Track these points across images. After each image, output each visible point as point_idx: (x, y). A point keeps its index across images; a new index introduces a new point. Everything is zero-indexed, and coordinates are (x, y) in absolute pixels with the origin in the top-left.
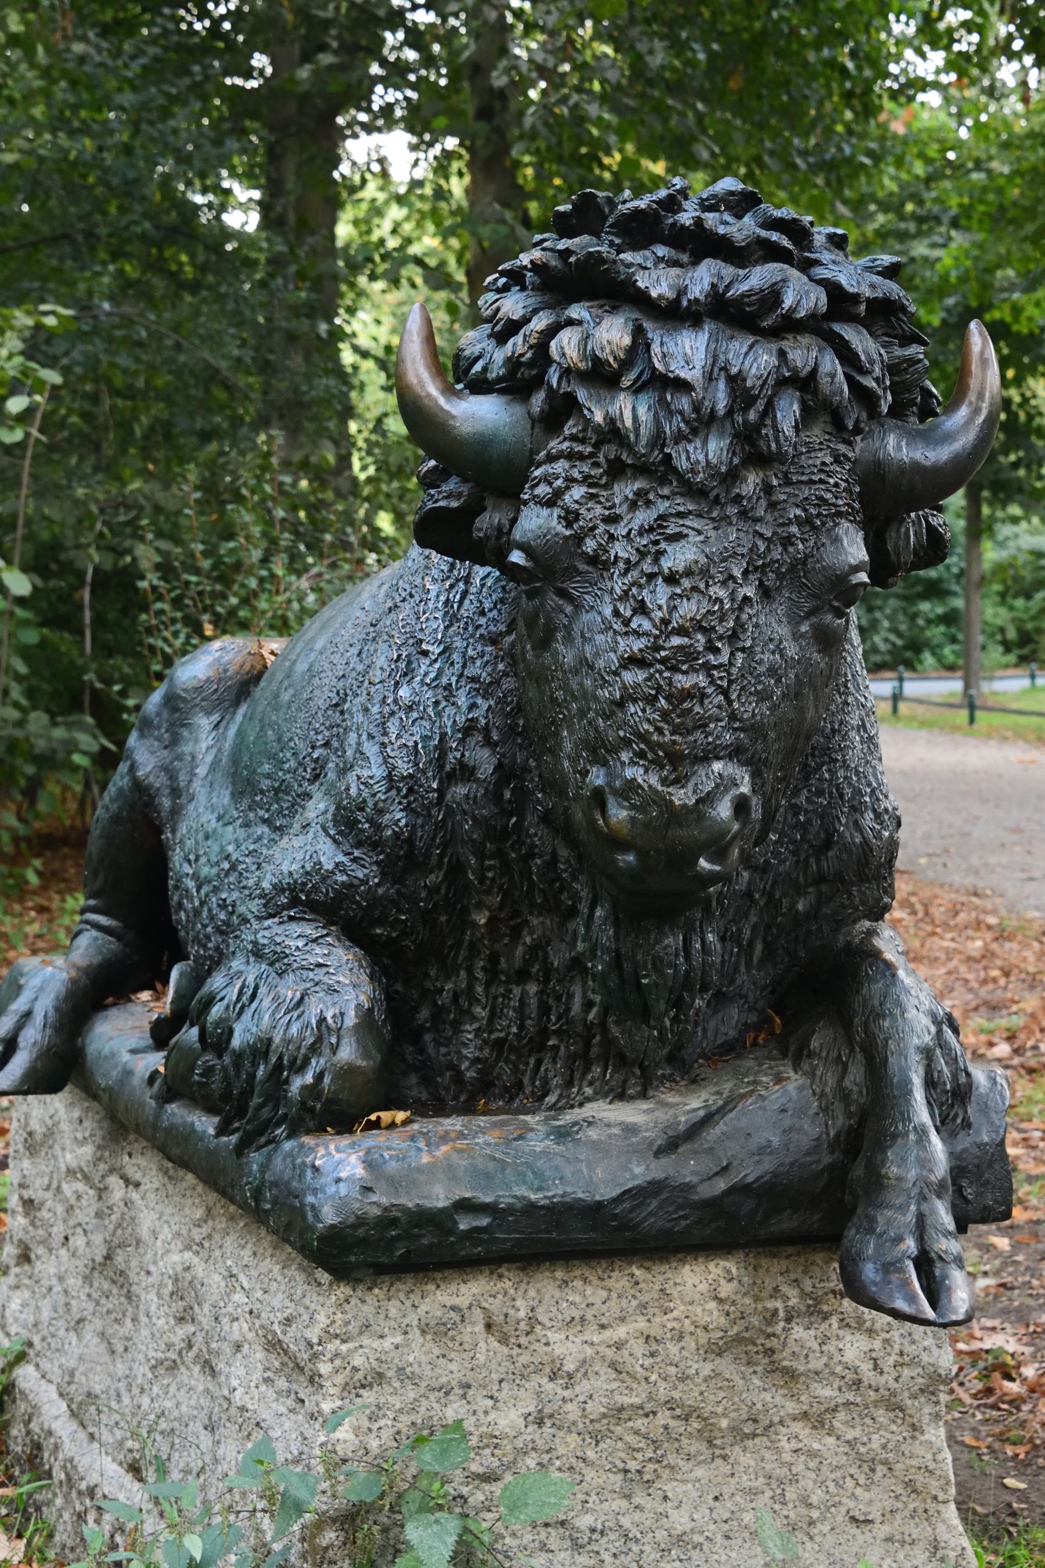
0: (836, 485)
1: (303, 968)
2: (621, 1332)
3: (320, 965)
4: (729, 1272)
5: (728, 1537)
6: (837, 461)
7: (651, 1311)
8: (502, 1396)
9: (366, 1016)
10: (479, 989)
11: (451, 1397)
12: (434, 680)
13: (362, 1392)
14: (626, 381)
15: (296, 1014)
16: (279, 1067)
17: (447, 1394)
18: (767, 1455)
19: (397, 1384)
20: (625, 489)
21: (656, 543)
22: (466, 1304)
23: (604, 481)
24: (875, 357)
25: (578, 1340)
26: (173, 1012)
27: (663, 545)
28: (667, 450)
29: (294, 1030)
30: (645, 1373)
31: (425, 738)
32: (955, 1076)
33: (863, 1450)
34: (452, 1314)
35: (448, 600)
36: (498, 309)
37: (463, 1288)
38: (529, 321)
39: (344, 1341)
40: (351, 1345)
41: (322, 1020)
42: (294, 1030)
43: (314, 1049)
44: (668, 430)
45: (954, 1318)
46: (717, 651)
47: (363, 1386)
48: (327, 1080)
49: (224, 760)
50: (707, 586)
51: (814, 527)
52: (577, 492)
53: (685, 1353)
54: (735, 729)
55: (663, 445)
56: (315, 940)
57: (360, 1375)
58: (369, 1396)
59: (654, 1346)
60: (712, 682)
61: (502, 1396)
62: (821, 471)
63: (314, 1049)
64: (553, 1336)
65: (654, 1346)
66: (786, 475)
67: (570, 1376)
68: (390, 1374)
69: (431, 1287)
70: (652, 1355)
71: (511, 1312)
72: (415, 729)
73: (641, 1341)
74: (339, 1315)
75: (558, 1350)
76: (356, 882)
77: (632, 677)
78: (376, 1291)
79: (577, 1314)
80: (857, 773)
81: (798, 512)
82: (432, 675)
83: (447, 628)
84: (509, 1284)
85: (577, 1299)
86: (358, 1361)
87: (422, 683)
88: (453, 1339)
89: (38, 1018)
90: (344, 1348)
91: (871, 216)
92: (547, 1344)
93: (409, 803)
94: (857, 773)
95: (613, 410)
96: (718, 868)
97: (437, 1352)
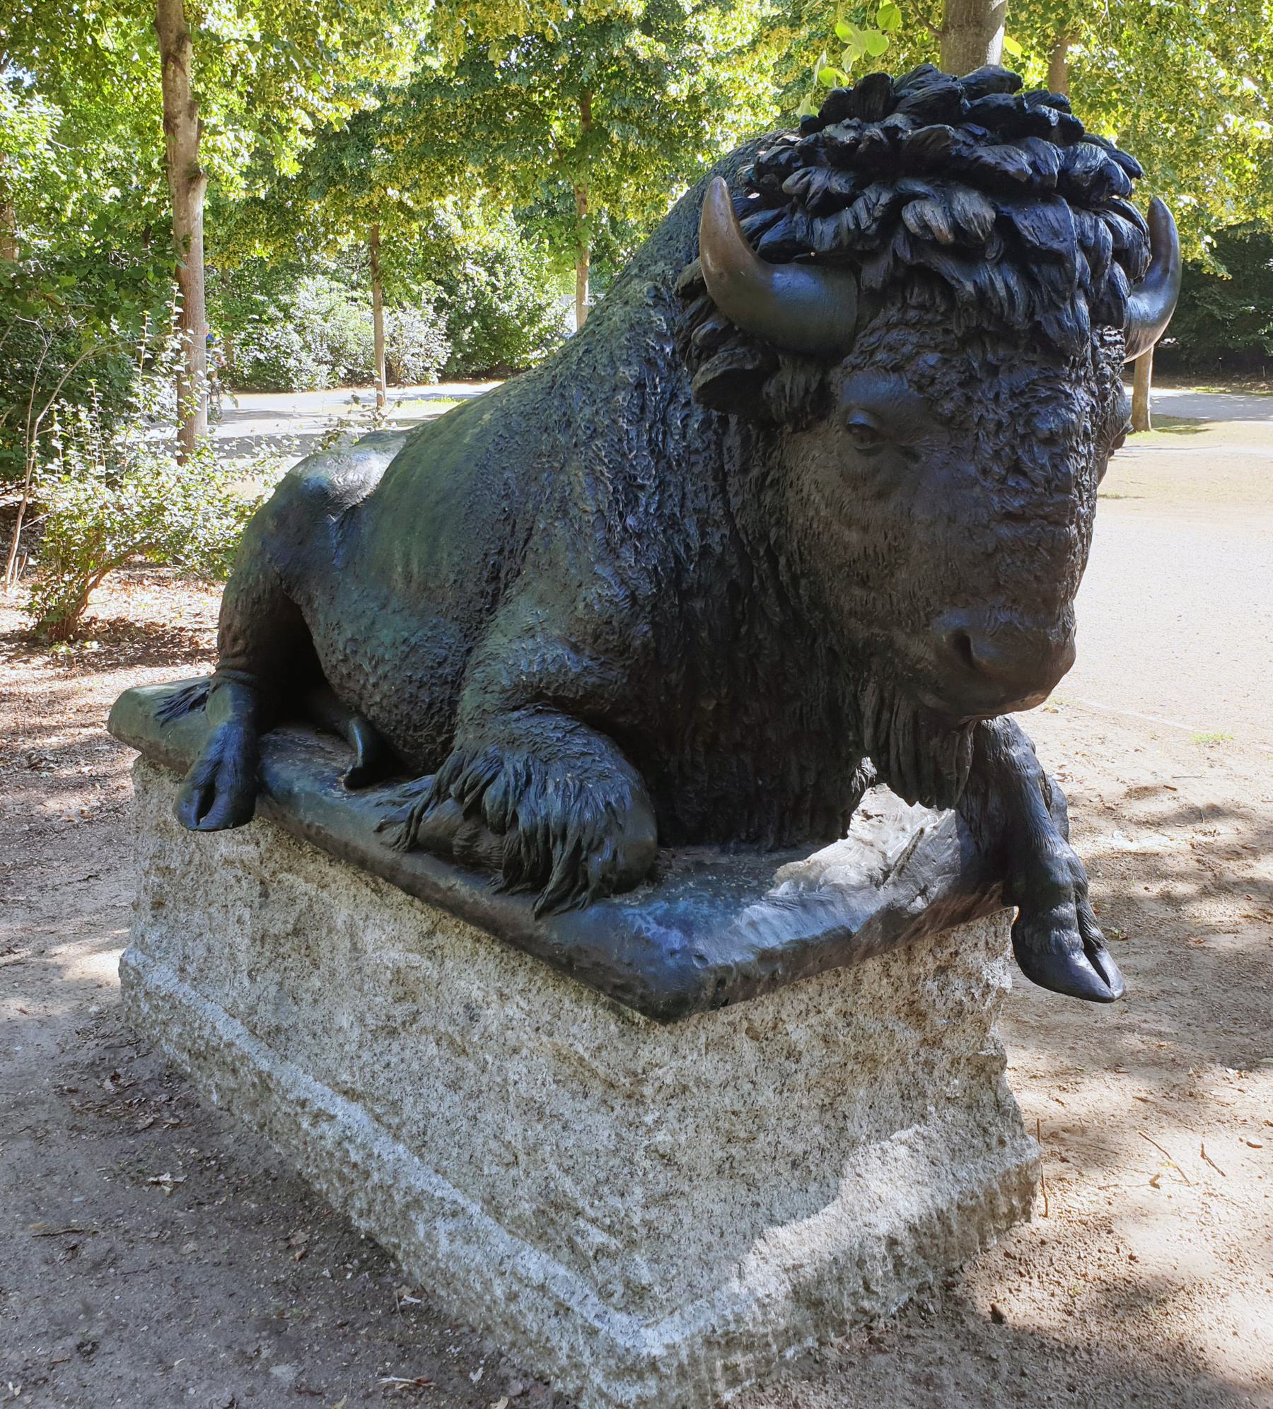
1: (569, 756)
3: (584, 754)
10: (701, 759)
12: (656, 510)
13: (671, 1101)
16: (578, 849)
18: (901, 1070)
19: (695, 1090)
21: (1027, 405)
26: (365, 763)
27: (1035, 408)
28: (1037, 318)
35: (650, 441)
36: (809, 184)
40: (665, 1069)
43: (607, 831)
48: (620, 858)
56: (571, 731)
64: (790, 1028)
68: (691, 1084)
70: (849, 1025)
72: (651, 554)
73: (841, 1016)
75: (794, 1037)
76: (606, 683)
77: (1005, 531)
83: (657, 463)
87: (646, 512)
88: (728, 1046)
90: (660, 1072)
95: (983, 278)
97: (717, 1058)
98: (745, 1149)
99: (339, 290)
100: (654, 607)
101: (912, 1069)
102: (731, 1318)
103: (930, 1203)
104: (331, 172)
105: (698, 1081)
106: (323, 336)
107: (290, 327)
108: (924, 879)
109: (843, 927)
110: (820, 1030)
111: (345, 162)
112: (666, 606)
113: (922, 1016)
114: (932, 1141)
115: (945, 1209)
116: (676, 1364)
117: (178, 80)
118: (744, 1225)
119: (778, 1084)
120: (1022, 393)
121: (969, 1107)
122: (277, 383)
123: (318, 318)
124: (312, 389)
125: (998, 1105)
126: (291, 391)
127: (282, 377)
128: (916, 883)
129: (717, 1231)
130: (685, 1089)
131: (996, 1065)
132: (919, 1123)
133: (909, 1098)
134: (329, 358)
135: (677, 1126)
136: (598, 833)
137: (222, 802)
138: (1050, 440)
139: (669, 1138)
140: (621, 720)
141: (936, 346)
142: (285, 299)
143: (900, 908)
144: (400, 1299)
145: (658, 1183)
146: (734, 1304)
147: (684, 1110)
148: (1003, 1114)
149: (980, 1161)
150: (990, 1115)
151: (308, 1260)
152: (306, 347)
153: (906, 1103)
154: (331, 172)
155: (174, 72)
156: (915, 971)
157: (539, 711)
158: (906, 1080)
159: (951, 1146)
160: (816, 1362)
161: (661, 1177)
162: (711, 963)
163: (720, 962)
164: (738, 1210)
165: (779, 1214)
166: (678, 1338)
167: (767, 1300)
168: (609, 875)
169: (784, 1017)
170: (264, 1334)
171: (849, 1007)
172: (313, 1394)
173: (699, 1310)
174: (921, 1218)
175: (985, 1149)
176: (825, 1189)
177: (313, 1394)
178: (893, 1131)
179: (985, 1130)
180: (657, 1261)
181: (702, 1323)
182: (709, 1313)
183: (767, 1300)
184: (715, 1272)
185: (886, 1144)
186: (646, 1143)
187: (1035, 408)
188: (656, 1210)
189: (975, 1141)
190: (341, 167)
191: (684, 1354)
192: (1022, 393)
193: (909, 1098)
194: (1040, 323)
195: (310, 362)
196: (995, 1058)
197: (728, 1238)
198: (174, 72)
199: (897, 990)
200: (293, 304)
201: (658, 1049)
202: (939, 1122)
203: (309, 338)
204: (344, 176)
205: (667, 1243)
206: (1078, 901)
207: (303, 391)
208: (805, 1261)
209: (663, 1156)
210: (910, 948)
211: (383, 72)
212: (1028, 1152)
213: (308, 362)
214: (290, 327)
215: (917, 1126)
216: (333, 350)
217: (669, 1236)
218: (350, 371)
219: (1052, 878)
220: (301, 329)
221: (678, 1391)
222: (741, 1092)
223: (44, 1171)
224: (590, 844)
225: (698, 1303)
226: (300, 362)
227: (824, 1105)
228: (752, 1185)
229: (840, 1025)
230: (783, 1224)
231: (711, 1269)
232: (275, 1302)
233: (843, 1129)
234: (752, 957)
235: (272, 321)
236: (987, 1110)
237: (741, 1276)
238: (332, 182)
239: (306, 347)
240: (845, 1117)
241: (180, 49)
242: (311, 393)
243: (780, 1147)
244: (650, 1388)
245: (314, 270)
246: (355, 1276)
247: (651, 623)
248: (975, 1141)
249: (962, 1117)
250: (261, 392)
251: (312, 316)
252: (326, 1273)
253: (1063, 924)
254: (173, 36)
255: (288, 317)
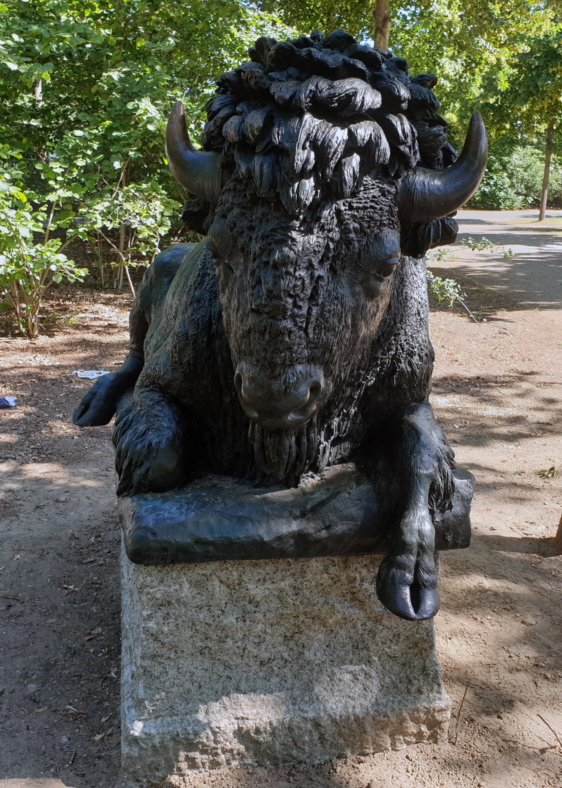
0: (381, 209)
2: (283, 584)
3: (156, 416)
4: (333, 561)
5: (331, 661)
6: (384, 195)
7: (296, 576)
8: (226, 610)
9: (172, 443)
11: (203, 610)
12: (210, 288)
14: (259, 149)
15: (140, 440)
17: (200, 609)
18: (352, 630)
19: (177, 605)
20: (259, 211)
21: (270, 244)
22: (209, 573)
23: (248, 206)
24: (410, 134)
25: (262, 588)
27: (273, 246)
28: (277, 190)
29: (139, 447)
30: (293, 602)
31: (203, 316)
32: (446, 485)
33: (395, 630)
34: (203, 577)
37: (208, 567)
38: (218, 112)
39: (151, 588)
40: (155, 589)
41: (150, 444)
42: (139, 447)
44: (278, 178)
45: (425, 616)
46: (300, 307)
47: (161, 605)
48: (150, 473)
49: (153, 306)
50: (295, 271)
51: (365, 233)
52: (236, 211)
53: (312, 594)
54: (311, 348)
55: (276, 188)
57: (160, 601)
58: (164, 610)
59: (298, 591)
60: (296, 325)
61: (226, 610)
62: (372, 201)
63: (147, 457)
64: (250, 586)
65: (298, 591)
66: (350, 204)
67: (258, 602)
68: (173, 601)
69: (192, 566)
70: (296, 594)
71: (231, 577)
74: (149, 578)
78: (166, 568)
79: (261, 577)
80: (412, 337)
81: (356, 225)
82: (210, 286)
84: (229, 565)
85: (262, 571)
86: (158, 596)
89: (98, 397)
90: (151, 590)
91: (308, 33)
92: (247, 590)
93: (194, 347)
94: (412, 337)
96: (300, 417)
97: (196, 592)
98: (218, 645)
99: (538, 155)
100: (195, 341)
101: (360, 632)
102: (191, 731)
103: (350, 710)
104: (531, 89)
105: (178, 601)
106: (523, 180)
107: (505, 174)
108: (329, 521)
109: (260, 536)
110: (276, 593)
111: (539, 83)
112: (200, 341)
113: (362, 603)
114: (370, 677)
115: (361, 717)
116: (150, 744)
117: (381, 42)
118: (219, 687)
119: (240, 615)
120: (267, 237)
121: (404, 665)
122: (492, 205)
123: (521, 170)
124: (512, 209)
125: (424, 669)
126: (499, 209)
127: (496, 202)
128: (323, 522)
129: (196, 684)
130: (169, 603)
131: (426, 646)
132: (366, 665)
133: (357, 648)
134: (524, 192)
135: (161, 621)
136: (141, 458)
137: (90, 413)
138: (275, 266)
139: (155, 626)
140: (184, 401)
141: (240, 205)
142: (506, 159)
143: (308, 534)
144: (109, 672)
145: (149, 648)
146: (195, 725)
147: (168, 614)
148: (426, 675)
149: (399, 698)
150: (417, 673)
151: (91, 642)
152: (512, 186)
153: (355, 650)
154: (531, 89)
155: (380, 38)
156: (352, 575)
157: (152, 390)
158: (357, 637)
159: (382, 683)
160: (248, 773)
161: (151, 645)
162: (159, 538)
163: (165, 538)
164: (215, 677)
165: (243, 686)
166: (153, 731)
167: (218, 730)
168: (143, 481)
169: (246, 579)
170: (42, 668)
171: (298, 584)
172: (35, 701)
173: (174, 722)
174: (341, 717)
175: (406, 691)
176: (283, 683)
177: (35, 701)
178: (344, 664)
179: (410, 681)
180: (149, 688)
181: (171, 729)
182: (178, 725)
183: (218, 730)
184: (190, 705)
185: (336, 670)
186: (143, 625)
187: (273, 246)
188: (149, 662)
189: (400, 685)
190: (537, 86)
191: (157, 741)
192: (267, 237)
193: (357, 648)
194: (279, 193)
195: (513, 194)
196: (425, 641)
197: (204, 690)
198: (380, 38)
199: (335, 583)
200: (509, 162)
201: (149, 578)
202: (380, 668)
203: (514, 181)
204: (538, 91)
205: (157, 681)
206: (418, 555)
207: (506, 210)
208: (250, 717)
209: (152, 635)
210: (346, 560)
211: (534, 29)
212: (438, 702)
213: (512, 193)
214: (505, 174)
215: (364, 666)
216: (527, 188)
217: (158, 678)
218: (535, 200)
219: (403, 537)
220: (510, 176)
221: (152, 759)
222: (213, 614)
223: (29, 570)
224: (137, 462)
225: (175, 718)
226: (507, 193)
227: (286, 636)
228: (227, 667)
229: (290, 593)
230: (245, 693)
231: (188, 703)
232: (61, 656)
233: (301, 653)
234: (189, 540)
235: (496, 171)
236: (416, 670)
237: (207, 713)
238: (531, 94)
239: (512, 186)
240: (304, 647)
241: (384, 25)
242: (511, 211)
243: (246, 651)
244: (134, 752)
245: (524, 144)
246: (103, 655)
247: (193, 349)
248: (400, 685)
249: (396, 668)
250: (483, 209)
251: (518, 169)
252: (92, 650)
253: (402, 567)
254: (381, 19)
255: (505, 169)
